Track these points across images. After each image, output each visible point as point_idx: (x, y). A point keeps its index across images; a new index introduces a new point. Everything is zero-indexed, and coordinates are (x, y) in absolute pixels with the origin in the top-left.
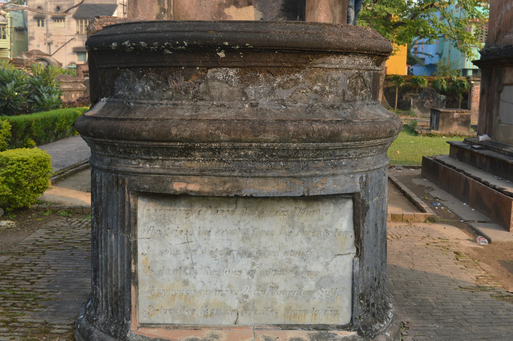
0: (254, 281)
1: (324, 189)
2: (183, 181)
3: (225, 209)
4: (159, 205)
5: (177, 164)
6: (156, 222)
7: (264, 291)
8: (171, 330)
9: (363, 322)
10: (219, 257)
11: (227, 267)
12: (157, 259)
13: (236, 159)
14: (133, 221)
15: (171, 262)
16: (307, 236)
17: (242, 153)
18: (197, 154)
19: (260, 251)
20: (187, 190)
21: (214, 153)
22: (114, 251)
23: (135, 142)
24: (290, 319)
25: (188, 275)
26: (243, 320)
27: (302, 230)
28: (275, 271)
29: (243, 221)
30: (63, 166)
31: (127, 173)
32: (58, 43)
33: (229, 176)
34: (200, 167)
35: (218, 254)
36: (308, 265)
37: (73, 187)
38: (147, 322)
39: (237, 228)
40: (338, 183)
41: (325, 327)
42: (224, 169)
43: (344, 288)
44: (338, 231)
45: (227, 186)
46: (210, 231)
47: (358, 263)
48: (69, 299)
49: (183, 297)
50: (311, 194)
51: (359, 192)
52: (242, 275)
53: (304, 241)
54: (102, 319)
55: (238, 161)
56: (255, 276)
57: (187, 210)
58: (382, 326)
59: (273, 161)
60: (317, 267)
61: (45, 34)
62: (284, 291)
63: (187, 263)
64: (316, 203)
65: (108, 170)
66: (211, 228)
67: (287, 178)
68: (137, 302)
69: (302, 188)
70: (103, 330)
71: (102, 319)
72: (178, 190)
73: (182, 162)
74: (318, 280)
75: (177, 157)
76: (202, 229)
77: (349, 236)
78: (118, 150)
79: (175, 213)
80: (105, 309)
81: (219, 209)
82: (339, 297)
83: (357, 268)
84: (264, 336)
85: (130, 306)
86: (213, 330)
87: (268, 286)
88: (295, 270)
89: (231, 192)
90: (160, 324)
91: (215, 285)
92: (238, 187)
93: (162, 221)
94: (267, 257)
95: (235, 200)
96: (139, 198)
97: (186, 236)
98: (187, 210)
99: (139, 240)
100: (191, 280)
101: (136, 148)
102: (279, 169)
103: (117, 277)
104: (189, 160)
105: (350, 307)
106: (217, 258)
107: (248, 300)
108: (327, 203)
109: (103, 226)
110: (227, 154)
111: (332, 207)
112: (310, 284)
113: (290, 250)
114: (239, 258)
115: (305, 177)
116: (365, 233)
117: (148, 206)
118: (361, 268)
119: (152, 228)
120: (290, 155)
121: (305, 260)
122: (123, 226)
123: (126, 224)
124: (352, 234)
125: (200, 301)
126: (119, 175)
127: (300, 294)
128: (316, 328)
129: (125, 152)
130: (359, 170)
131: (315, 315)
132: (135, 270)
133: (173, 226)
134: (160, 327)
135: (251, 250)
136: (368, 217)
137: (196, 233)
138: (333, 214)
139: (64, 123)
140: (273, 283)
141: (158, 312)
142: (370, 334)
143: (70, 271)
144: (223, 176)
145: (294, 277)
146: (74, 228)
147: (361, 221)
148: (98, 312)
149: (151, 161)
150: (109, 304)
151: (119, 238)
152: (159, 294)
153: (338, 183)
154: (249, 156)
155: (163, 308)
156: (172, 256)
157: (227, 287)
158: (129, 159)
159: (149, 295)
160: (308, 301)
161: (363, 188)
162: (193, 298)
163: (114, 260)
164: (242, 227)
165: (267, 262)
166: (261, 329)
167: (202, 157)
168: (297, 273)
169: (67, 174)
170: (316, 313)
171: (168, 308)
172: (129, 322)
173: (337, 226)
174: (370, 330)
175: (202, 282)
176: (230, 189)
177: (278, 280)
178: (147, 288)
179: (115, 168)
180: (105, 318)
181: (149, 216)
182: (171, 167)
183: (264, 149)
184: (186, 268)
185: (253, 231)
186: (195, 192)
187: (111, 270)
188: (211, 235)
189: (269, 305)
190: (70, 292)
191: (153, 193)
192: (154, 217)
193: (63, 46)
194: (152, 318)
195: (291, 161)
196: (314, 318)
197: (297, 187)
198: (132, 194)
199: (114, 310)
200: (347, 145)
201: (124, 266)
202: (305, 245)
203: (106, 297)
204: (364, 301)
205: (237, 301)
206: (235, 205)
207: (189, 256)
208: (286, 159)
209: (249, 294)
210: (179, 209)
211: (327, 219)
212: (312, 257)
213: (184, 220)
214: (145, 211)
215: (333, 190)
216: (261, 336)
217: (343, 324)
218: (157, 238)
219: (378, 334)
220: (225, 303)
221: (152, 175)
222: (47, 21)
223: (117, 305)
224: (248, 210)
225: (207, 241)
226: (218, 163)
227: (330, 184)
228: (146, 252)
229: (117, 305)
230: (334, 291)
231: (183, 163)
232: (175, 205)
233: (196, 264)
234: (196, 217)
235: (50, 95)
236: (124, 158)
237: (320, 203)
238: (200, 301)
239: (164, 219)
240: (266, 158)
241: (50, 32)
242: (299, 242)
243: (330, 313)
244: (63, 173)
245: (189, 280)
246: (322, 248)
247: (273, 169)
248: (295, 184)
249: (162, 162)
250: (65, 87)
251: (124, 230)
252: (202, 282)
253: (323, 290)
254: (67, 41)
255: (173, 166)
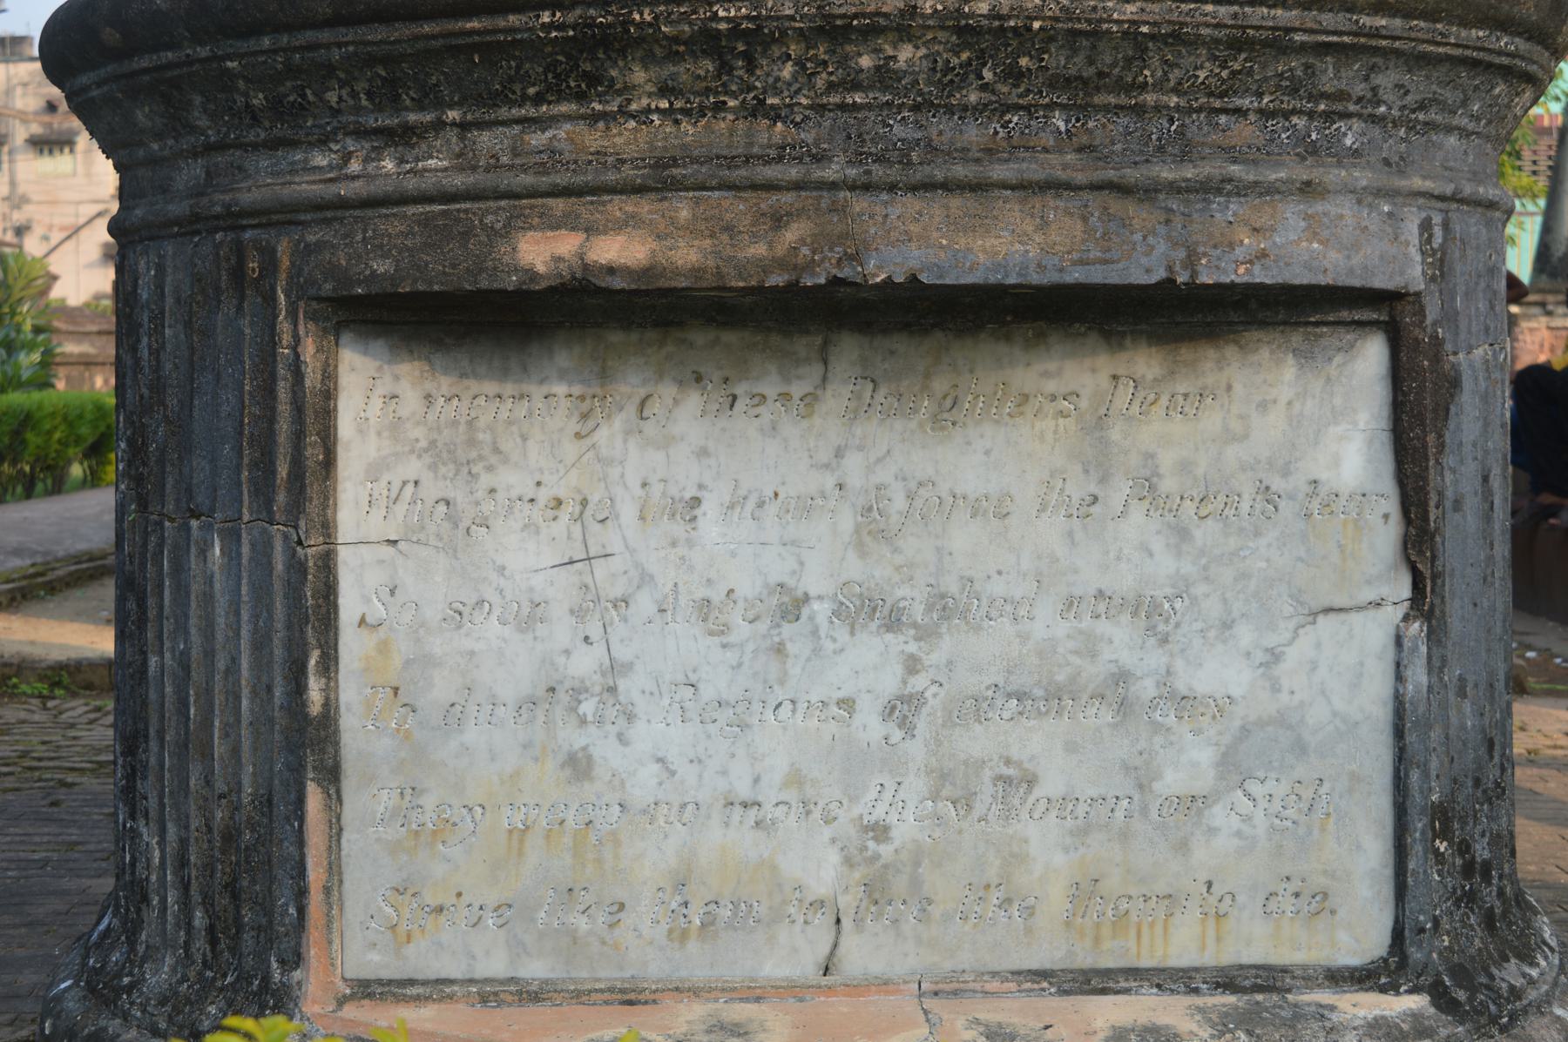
0: (916, 750)
1: (1263, 255)
2: (567, 223)
3: (770, 388)
4: (446, 372)
5: (537, 139)
6: (427, 459)
7: (964, 802)
8: (506, 1010)
9: (1450, 949)
10: (741, 630)
11: (782, 683)
12: (437, 645)
13: (835, 99)
14: (313, 453)
15: (506, 661)
16: (1169, 518)
17: (866, 62)
18: (639, 76)
19: (943, 596)
20: (586, 267)
21: (725, 68)
22: (221, 621)
23: (325, 36)
24: (1097, 940)
25: (592, 729)
26: (864, 954)
27: (1148, 488)
28: (1020, 697)
29: (860, 448)
30: (45, 553)
31: (285, 215)
32: (50, 227)
33: (797, 186)
34: (653, 148)
35: (736, 618)
36: (1179, 664)
37: (78, 616)
38: (385, 974)
39: (830, 481)
40: (1325, 234)
41: (1268, 979)
42: (773, 153)
43: (1354, 778)
44: (1323, 491)
45: (791, 235)
46: (696, 502)
47: (1424, 649)
48: (20, 952)
49: (567, 840)
50: (1206, 278)
51: (1418, 294)
52: (858, 719)
53: (1157, 545)
54: (159, 976)
55: (842, 107)
56: (922, 725)
57: (582, 398)
58: (1534, 973)
59: (1017, 108)
60: (1221, 673)
61: (4, 199)
62: (1067, 801)
63: (584, 664)
64: (1211, 353)
65: (195, 218)
66: (701, 487)
67: (1086, 195)
68: (334, 868)
69: (1161, 247)
70: (163, 1025)
71: (159, 976)
72: (541, 268)
73: (562, 131)
74: (1227, 739)
75: (538, 100)
76: (656, 489)
77: (1374, 518)
78: (241, 100)
79: (522, 409)
80: (177, 925)
81: (740, 389)
82: (1331, 826)
83: (1418, 676)
84: (977, 1022)
85: (301, 893)
86: (720, 1005)
87: (987, 774)
88: (1117, 690)
89: (810, 266)
90: (452, 982)
91: (724, 773)
92: (844, 236)
93: (461, 455)
94: (978, 629)
95: (819, 340)
96: (346, 338)
97: (577, 530)
98: (582, 398)
99: (344, 555)
100: (607, 753)
101: (330, 69)
102: (1046, 150)
103: (236, 751)
104: (595, 118)
105: (1389, 872)
106: (732, 638)
107: (886, 850)
108: (1265, 353)
109: (170, 507)
110: (787, 71)
111: (1289, 370)
112: (1189, 762)
113: (1092, 592)
114: (842, 634)
115: (1174, 188)
116: (1448, 504)
117: (388, 378)
118: (1435, 679)
119: (410, 488)
120: (1101, 74)
121: (1164, 641)
122: (264, 490)
123: (283, 470)
124: (1390, 504)
125: (651, 858)
126: (248, 235)
127: (1144, 810)
128: (1227, 980)
129: (277, 107)
130: (1418, 183)
131: (1218, 916)
132: (326, 704)
133: (512, 480)
134: (451, 997)
135: (900, 593)
136: (1459, 428)
137: (628, 512)
138: (1297, 406)
139: (57, 435)
140: (1008, 762)
141: (442, 919)
142: (1492, 1008)
143: (36, 856)
144: (771, 187)
145: (1115, 726)
146: (72, 726)
147: (1431, 438)
148: (141, 949)
149: (402, 138)
150: (196, 896)
151: (245, 549)
152: (444, 828)
153: (1325, 234)
154: (898, 76)
155: (466, 899)
156: (507, 631)
157: (786, 784)
158: (293, 144)
159: (393, 832)
160: (1183, 847)
161: (1433, 279)
162: (617, 843)
163: (221, 664)
164: (855, 480)
165: (977, 654)
166: (955, 993)
167: (664, 91)
168: (1124, 706)
169: (60, 579)
170: (1223, 908)
171: (492, 897)
172: (297, 975)
173: (1315, 465)
174: (1488, 987)
175: (660, 760)
176: (805, 251)
177: (1033, 739)
178: (386, 800)
179: (227, 198)
180: (174, 970)
181: (395, 427)
182: (505, 160)
183: (976, 31)
184: (579, 692)
185: (910, 497)
186: (626, 271)
187: (207, 724)
188: (701, 522)
189: (992, 875)
190: (30, 924)
191: (414, 295)
192: (418, 433)
193: (69, 237)
194: (410, 950)
195: (1106, 109)
196: (1211, 933)
197: (1138, 237)
198: (313, 317)
199: (219, 926)
200: (1376, 33)
201: (269, 689)
202: (1165, 565)
203: (182, 862)
204: (1451, 844)
205: (834, 857)
206: (816, 370)
207: (595, 631)
208: (1078, 93)
209: (892, 819)
210: (545, 389)
211: (1270, 430)
212: (1199, 625)
213: (570, 449)
214: (378, 407)
215: (1307, 266)
216: (960, 1023)
217: (1354, 961)
218: (433, 541)
219: (1525, 1011)
220: (774, 868)
221: (411, 210)
222: (10, 153)
223: (235, 897)
224: (882, 391)
225: (681, 550)
226: (741, 125)
227: (1293, 237)
228: (378, 611)
229: (235, 897)
230: (1307, 794)
231: (567, 134)
232: (525, 369)
233: (628, 667)
234: (628, 433)
235: (9, 354)
236: (274, 144)
237: (1230, 351)
238: (651, 858)
239: (472, 442)
240: (984, 87)
241: (21, 189)
242: (1136, 551)
243: (1288, 904)
244: (42, 574)
245: (596, 752)
246: (1244, 576)
247: (1017, 148)
248: (1125, 223)
249: (462, 138)
250: (71, 348)
251: (269, 502)
252: (660, 760)
253: (1255, 788)
254: (82, 220)
255: (515, 153)
